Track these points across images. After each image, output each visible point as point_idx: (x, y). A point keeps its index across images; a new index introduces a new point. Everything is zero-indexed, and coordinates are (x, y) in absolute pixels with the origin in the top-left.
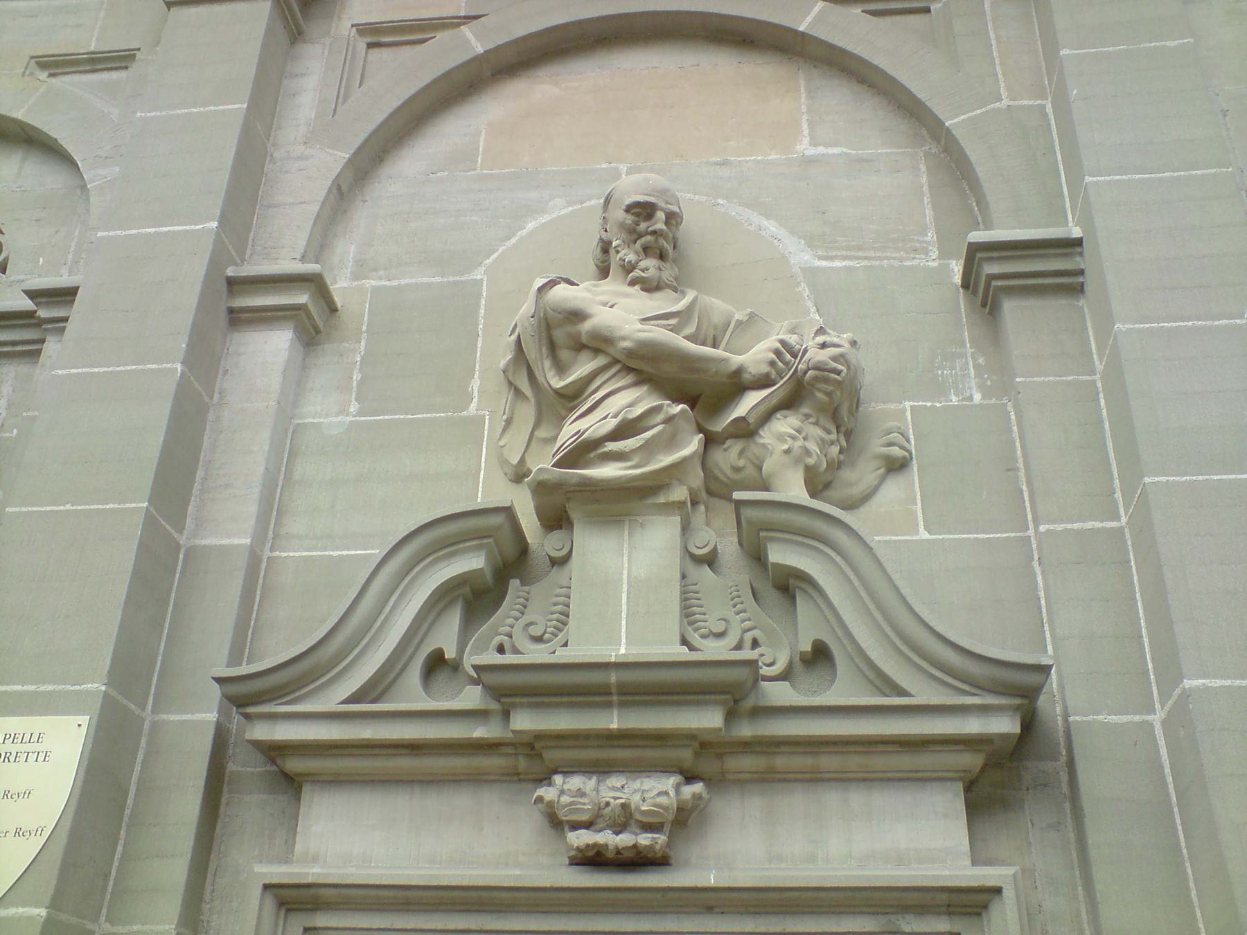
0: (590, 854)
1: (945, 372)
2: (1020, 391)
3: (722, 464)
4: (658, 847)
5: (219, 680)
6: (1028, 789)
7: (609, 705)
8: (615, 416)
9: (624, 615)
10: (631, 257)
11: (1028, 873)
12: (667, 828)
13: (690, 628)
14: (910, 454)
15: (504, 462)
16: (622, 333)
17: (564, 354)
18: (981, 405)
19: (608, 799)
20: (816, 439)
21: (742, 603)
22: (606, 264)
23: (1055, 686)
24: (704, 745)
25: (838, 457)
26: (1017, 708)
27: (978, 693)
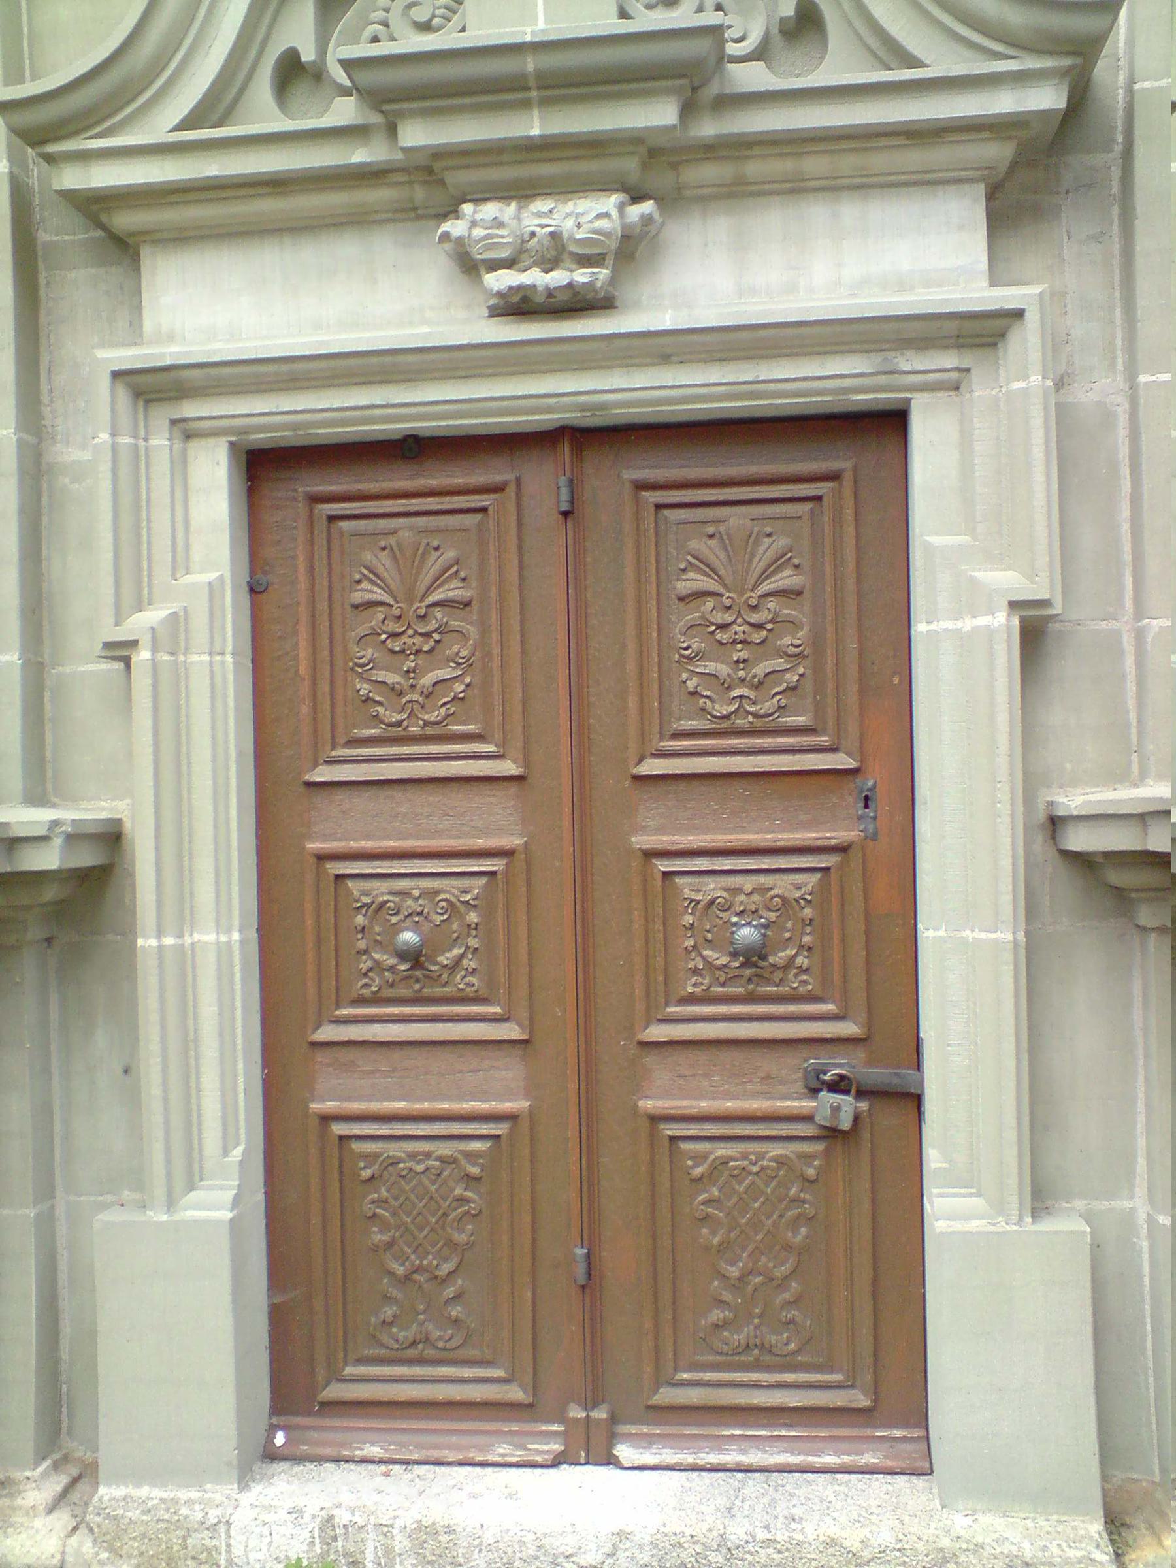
0: (515, 299)
4: (599, 284)
6: (1067, 192)
7: (526, 104)
11: (1057, 296)
12: (610, 261)
19: (532, 228)
23: (1121, 44)
24: (654, 153)
26: (1065, 73)
27: (1014, 54)
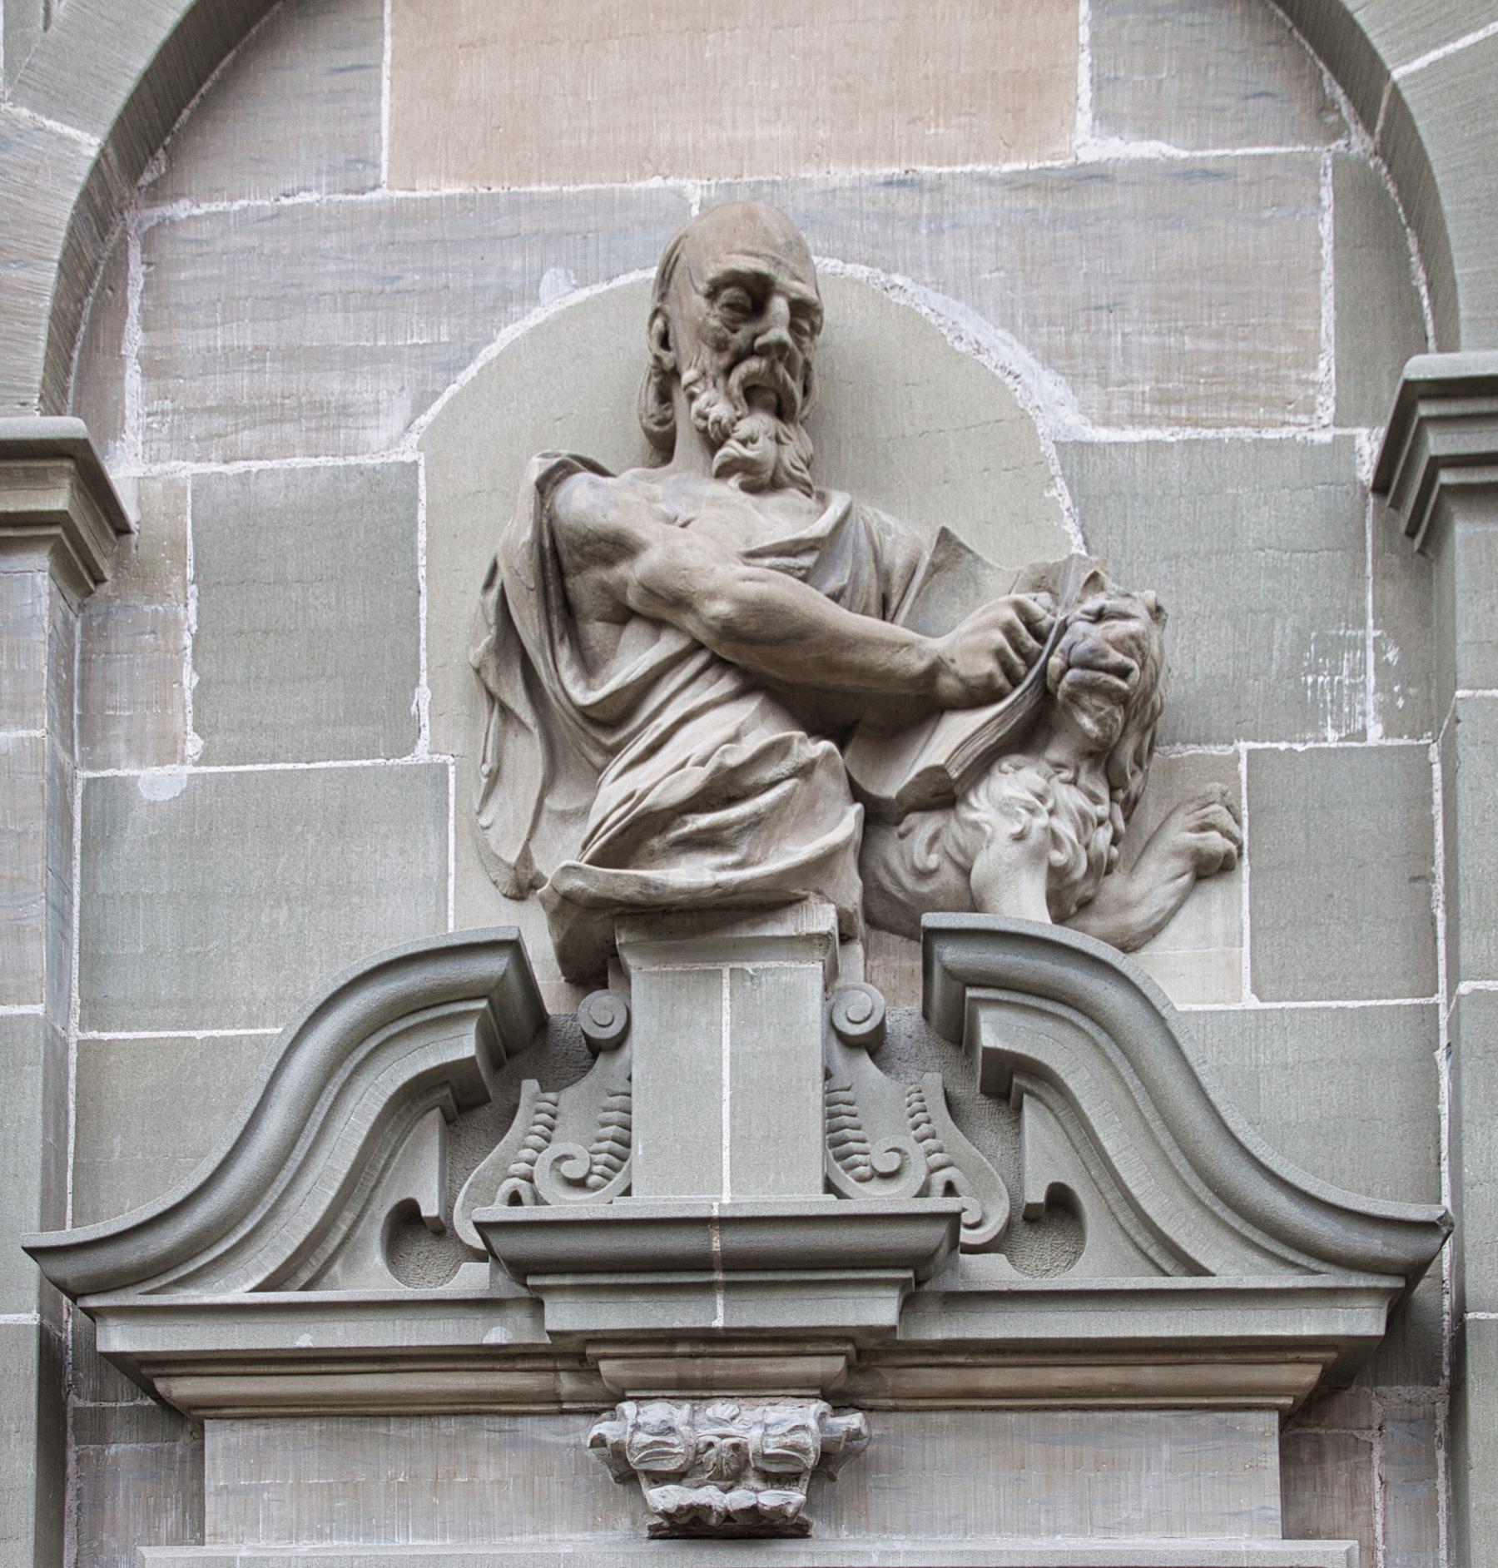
1: (1321, 679)
2: (1460, 717)
3: (895, 862)
5: (34, 1252)
8: (703, 763)
9: (726, 1142)
10: (721, 410)
13: (838, 1165)
14: (1240, 848)
15: (488, 859)
16: (710, 584)
17: (596, 631)
18: (1380, 750)
20: (1070, 813)
21: (928, 1122)
22: (667, 427)
23: (1446, 1265)
25: (1109, 852)
